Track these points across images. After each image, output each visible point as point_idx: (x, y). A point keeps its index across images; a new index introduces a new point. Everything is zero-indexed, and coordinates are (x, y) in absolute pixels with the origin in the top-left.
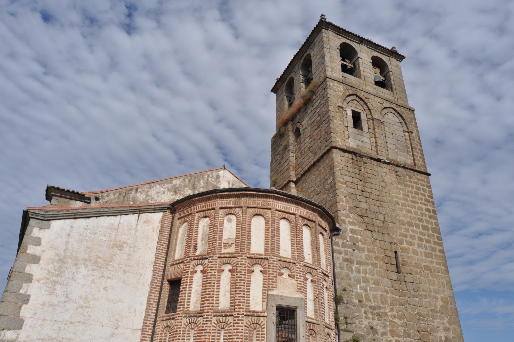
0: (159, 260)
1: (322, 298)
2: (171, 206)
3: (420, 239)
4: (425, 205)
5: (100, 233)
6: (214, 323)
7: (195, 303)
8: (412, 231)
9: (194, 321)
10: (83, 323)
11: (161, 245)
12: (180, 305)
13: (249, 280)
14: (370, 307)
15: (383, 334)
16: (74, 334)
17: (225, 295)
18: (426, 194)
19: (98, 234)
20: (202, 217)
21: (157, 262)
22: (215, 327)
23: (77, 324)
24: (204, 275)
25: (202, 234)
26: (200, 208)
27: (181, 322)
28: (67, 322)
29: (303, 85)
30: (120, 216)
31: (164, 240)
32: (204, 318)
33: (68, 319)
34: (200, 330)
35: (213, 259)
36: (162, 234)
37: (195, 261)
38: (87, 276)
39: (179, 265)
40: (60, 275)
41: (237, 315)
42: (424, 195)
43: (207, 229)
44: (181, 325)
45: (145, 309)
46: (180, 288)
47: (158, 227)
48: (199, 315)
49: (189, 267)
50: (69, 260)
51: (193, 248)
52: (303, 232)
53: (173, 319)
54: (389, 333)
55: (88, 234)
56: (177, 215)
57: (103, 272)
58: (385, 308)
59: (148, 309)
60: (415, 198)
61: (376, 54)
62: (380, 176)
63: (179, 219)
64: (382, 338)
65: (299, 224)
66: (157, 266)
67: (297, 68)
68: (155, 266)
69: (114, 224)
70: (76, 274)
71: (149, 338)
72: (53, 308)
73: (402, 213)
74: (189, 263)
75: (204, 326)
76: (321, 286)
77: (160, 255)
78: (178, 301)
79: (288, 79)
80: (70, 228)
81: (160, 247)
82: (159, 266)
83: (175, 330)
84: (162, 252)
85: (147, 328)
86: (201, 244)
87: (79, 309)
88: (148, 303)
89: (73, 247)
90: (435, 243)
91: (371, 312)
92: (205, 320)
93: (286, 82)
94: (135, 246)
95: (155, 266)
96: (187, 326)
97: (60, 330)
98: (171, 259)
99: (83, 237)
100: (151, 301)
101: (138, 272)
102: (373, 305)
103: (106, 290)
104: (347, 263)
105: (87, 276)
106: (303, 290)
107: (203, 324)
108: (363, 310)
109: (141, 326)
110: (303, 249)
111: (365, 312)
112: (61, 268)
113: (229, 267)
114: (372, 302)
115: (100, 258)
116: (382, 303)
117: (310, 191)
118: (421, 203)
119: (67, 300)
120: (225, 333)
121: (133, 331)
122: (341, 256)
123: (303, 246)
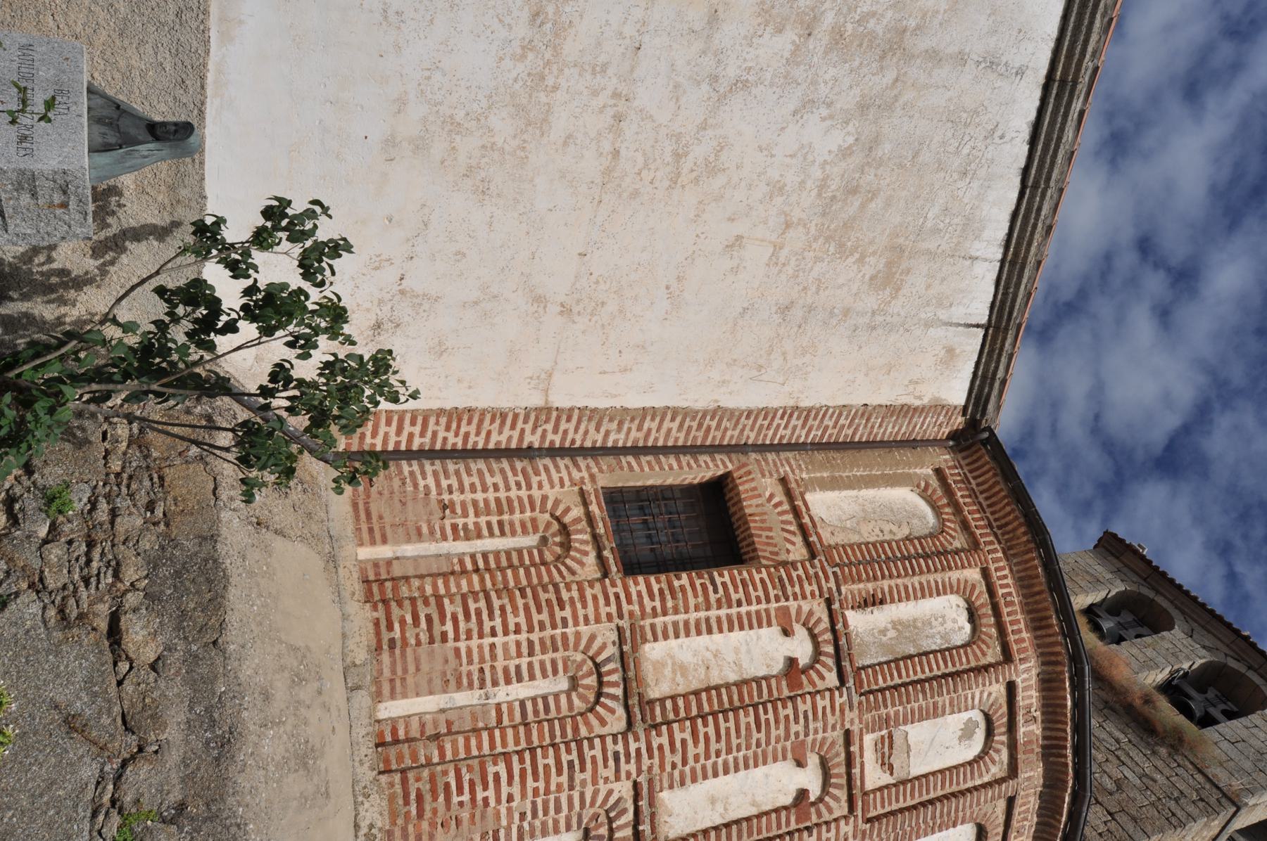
0: (800, 422)
2: (986, 435)
5: (961, 193)
6: (610, 792)
7: (674, 664)
10: (608, 172)
16: (568, 139)
17: (713, 801)
19: (961, 184)
20: (968, 601)
22: (593, 804)
23: (607, 147)
25: (915, 620)
27: (598, 621)
28: (623, 101)
29: (1161, 676)
30: (1000, 256)
31: (870, 425)
32: (624, 734)
33: (636, 103)
35: (842, 711)
37: (825, 623)
38: (805, 159)
40: (837, 43)
43: (933, 637)
44: (587, 621)
45: (626, 405)
47: (920, 398)
48: (637, 710)
49: (804, 597)
50: (890, 76)
51: (868, 592)
55: (971, 143)
56: (944, 458)
57: (805, 226)
59: (622, 415)
63: (938, 472)
69: (977, 242)
70: (824, 112)
72: (697, 27)
74: (817, 593)
80: (1017, 65)
86: (882, 626)
87: (675, 146)
88: (644, 413)
89: (938, 87)
94: (874, 328)
96: (584, 652)
97: (594, 73)
98: (804, 476)
99: (966, 125)
100: (653, 419)
101: (772, 357)
103: (732, 246)
105: (805, 159)
109: (560, 400)
112: (865, 45)
115: (863, 206)
119: (723, 87)
121: (543, 376)
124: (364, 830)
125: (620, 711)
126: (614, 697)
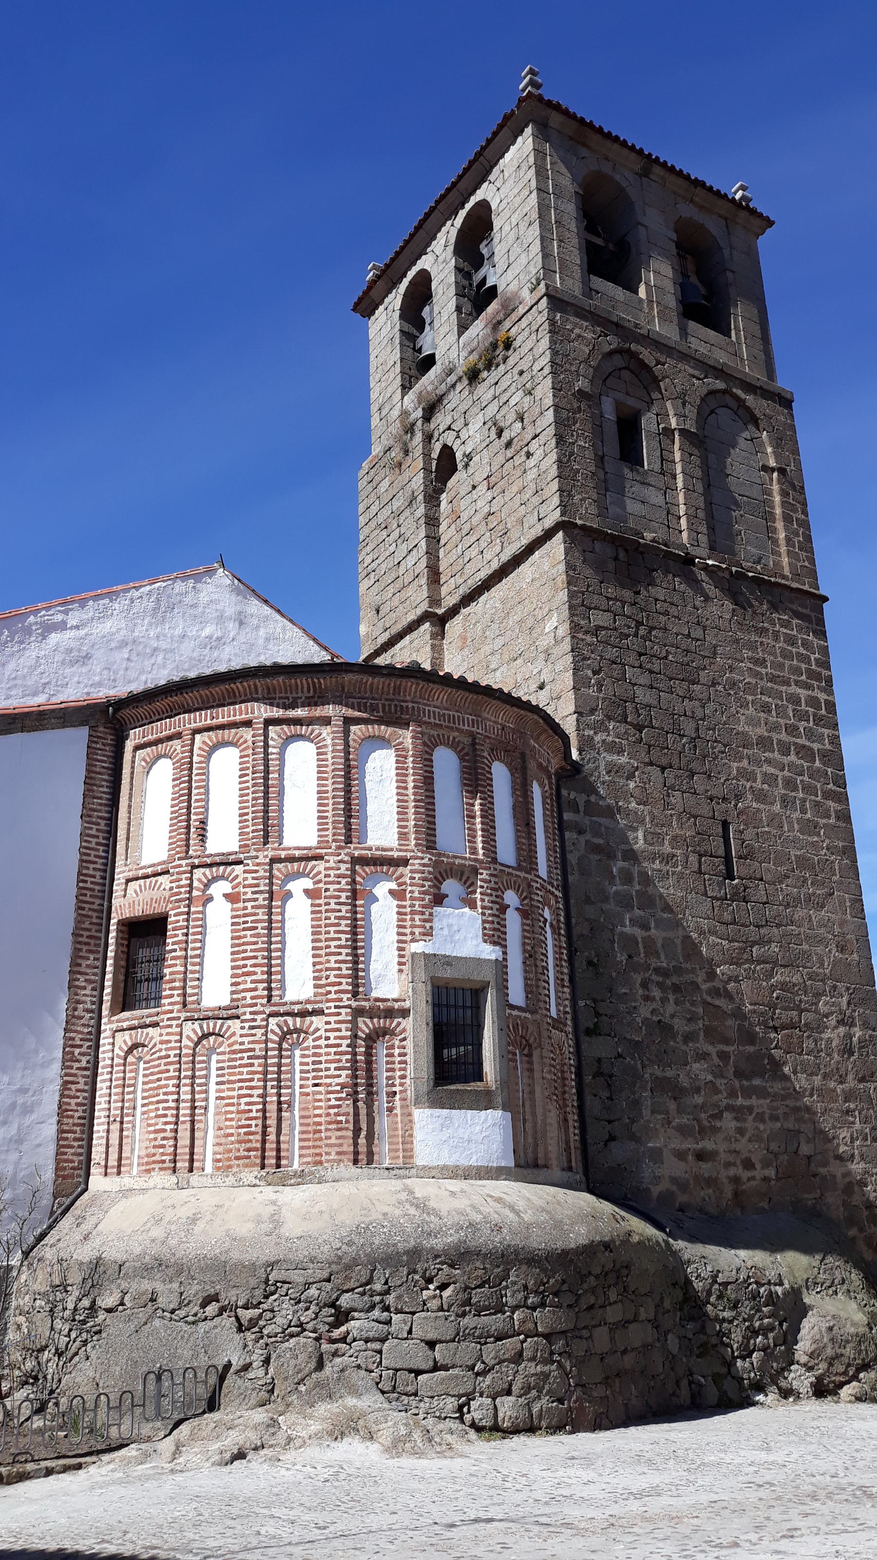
0: (91, 866)
1: (543, 954)
3: (790, 784)
4: (808, 687)
8: (769, 761)
9: (214, 1028)
11: (93, 823)
12: (171, 989)
13: (401, 930)
14: (657, 970)
15: (689, 1037)
18: (812, 657)
21: (85, 872)
24: (235, 906)
26: (206, 720)
34: (234, 1052)
36: (93, 791)
37: (207, 871)
39: (153, 879)
41: (333, 1010)
42: (806, 659)
46: (164, 943)
52: (494, 783)
53: (155, 1025)
54: (702, 1034)
58: (693, 971)
60: (781, 666)
61: (687, 211)
62: (689, 608)
64: (684, 1047)
65: (483, 763)
66: (86, 882)
67: (443, 242)
68: (81, 884)
71: (84, 1076)
73: (746, 712)
75: (246, 1040)
76: (541, 924)
77: (93, 853)
78: (162, 978)
79: (411, 274)
81: (91, 829)
82: (92, 883)
83: (163, 1053)
84: (97, 844)
85: (77, 1051)
90: (827, 795)
91: (658, 983)
92: (247, 1025)
93: (405, 282)
95: (81, 884)
102: (665, 965)
104: (597, 857)
106: (499, 937)
107: (241, 1036)
108: (638, 978)
110: (494, 828)
111: (645, 985)
113: (306, 883)
114: (663, 957)
116: (688, 957)
117: (487, 649)
118: (797, 683)
120: (303, 1056)
122: (583, 839)
123: (494, 821)
124: (258, 1182)
125: (230, 1022)
126: (222, 1026)
